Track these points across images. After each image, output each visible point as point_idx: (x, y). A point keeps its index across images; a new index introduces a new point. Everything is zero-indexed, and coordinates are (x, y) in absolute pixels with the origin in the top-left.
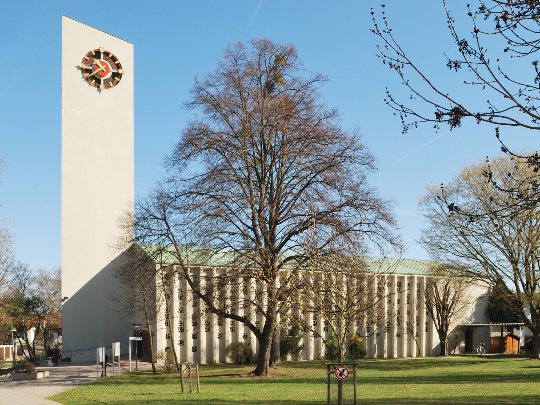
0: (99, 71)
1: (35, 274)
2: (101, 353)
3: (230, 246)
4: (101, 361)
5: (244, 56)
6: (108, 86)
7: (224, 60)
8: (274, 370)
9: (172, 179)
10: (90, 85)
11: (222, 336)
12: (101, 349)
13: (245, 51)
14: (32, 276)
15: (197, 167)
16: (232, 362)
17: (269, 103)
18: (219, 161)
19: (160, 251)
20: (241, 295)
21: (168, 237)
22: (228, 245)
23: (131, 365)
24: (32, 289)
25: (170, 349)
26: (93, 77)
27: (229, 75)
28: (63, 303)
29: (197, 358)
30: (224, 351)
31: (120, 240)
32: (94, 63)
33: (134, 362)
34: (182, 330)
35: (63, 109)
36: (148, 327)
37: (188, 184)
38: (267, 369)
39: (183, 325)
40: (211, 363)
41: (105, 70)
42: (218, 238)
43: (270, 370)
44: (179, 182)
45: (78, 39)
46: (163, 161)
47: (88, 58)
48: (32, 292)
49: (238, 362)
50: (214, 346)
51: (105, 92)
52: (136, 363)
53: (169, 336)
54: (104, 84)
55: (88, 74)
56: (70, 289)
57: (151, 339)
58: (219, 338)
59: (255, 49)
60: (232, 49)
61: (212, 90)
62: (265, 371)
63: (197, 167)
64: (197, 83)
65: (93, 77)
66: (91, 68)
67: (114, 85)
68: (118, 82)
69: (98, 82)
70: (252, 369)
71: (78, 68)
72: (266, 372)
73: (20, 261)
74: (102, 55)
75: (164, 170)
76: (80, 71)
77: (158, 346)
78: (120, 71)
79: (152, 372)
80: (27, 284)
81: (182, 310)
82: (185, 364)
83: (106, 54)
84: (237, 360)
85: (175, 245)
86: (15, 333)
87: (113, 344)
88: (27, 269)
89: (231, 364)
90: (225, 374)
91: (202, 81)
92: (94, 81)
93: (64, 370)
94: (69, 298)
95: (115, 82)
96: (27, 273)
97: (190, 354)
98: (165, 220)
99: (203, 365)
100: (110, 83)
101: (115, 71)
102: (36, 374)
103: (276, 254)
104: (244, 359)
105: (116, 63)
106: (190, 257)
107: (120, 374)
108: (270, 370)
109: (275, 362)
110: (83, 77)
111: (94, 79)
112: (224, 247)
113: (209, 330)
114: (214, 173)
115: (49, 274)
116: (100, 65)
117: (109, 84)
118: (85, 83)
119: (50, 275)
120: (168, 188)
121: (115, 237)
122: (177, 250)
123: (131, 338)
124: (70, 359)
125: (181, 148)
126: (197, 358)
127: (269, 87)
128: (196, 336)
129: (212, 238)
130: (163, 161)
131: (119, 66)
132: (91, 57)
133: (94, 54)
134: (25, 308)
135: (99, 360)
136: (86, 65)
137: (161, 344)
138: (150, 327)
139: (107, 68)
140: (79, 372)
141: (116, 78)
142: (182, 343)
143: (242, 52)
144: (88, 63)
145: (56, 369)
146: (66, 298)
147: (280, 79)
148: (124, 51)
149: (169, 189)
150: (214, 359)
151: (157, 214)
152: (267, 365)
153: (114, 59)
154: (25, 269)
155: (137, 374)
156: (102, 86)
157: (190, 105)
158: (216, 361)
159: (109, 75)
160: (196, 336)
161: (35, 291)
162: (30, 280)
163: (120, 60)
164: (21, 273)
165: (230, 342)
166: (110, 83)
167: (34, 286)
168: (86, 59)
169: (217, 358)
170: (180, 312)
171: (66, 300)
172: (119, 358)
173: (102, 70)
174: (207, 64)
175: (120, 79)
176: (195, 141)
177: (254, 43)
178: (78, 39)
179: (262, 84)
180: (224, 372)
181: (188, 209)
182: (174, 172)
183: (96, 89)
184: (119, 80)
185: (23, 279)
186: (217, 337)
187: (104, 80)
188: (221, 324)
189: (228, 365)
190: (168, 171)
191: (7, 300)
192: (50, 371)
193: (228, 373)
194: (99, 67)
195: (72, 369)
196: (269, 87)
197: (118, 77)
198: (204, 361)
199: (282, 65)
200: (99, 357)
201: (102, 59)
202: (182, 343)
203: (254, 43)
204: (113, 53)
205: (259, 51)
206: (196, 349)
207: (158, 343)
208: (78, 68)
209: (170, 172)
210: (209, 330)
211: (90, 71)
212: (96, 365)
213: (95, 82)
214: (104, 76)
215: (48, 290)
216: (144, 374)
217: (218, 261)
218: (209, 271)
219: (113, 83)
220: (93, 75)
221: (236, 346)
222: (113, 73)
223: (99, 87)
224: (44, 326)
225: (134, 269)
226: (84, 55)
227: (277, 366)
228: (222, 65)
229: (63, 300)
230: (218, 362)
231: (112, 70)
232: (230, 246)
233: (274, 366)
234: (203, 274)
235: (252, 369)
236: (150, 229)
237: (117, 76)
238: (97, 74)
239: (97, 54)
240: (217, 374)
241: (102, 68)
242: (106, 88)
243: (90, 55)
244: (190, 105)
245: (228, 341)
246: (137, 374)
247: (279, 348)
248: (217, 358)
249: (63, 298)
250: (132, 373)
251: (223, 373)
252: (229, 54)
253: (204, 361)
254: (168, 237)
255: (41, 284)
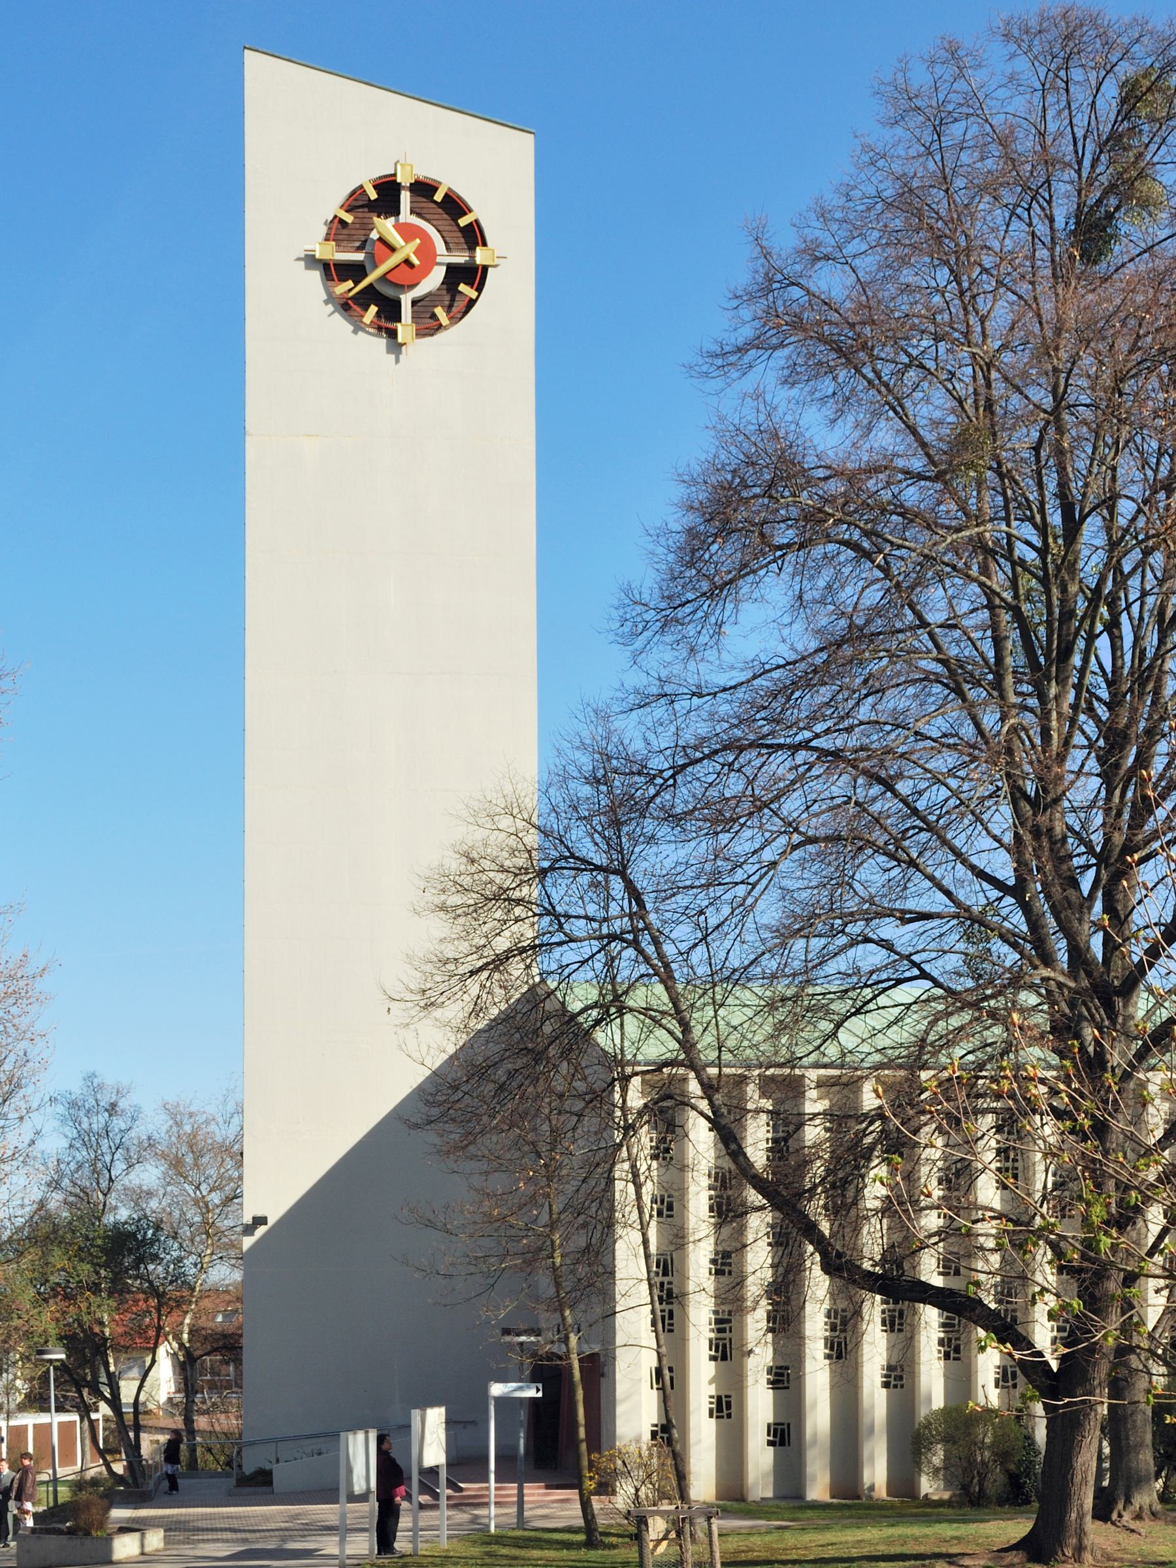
0: (395, 266)
1: (153, 1123)
2: (360, 1455)
3: (924, 975)
4: (359, 1487)
5: (973, 105)
6: (428, 327)
7: (881, 137)
8: (1123, 1537)
9: (655, 690)
10: (358, 328)
11: (900, 1375)
12: (361, 1436)
13: (977, 77)
14: (140, 1131)
15: (766, 624)
16: (946, 1496)
17: (1081, 302)
18: (863, 591)
19: (613, 1005)
20: (988, 1192)
21: (635, 944)
22: (916, 972)
23: (498, 1502)
24: (142, 1188)
25: (669, 1434)
26: (369, 296)
27: (908, 199)
28: (248, 1242)
29: (790, 1473)
30: (910, 1442)
31: (429, 968)
32: (374, 235)
33: (512, 1489)
34: (726, 1349)
35: (248, 439)
36: (566, 1340)
37: (724, 709)
38: (1081, 1533)
39: (727, 1325)
40: (850, 1498)
41: (416, 261)
42: (867, 940)
43: (1098, 1535)
44: (686, 704)
45: (311, 137)
46: (615, 614)
47: (349, 218)
48: (139, 1196)
49: (971, 1499)
50: (865, 1421)
51: (420, 351)
52: (521, 1495)
53: (669, 1380)
54: (416, 317)
55: (350, 284)
56: (273, 1189)
57: (580, 1394)
58: (886, 1385)
59: (1022, 64)
60: (920, 78)
61: (832, 282)
62: (1073, 1541)
63: (766, 624)
64: (767, 255)
65: (369, 296)
66: (359, 257)
67: (455, 319)
68: (472, 303)
69: (390, 310)
70: (1017, 1528)
71: (311, 261)
72: (1080, 1549)
73: (94, 1075)
74: (405, 198)
75: (621, 656)
76: (316, 275)
77: (619, 1423)
78: (481, 256)
79: (581, 1537)
80: (119, 1167)
81: (727, 1264)
82: (662, 1514)
83: (423, 189)
84: (965, 1488)
85: (667, 979)
86: (62, 1367)
87: (416, 1414)
88: (123, 1104)
89: (940, 1503)
90: (897, 1549)
91: (785, 242)
92: (373, 309)
93: (235, 1524)
94: (271, 1221)
95: (460, 304)
96: (119, 1123)
97: (760, 1457)
98: (622, 872)
99: (816, 1506)
100: (440, 312)
101: (460, 259)
102: (108, 1540)
103: (1119, 1002)
104: (996, 1480)
105: (463, 222)
106: (737, 1024)
107: (445, 1544)
108: (1098, 1535)
109: (1128, 1501)
110: (331, 298)
111: (369, 296)
112: (899, 982)
113: (843, 1349)
114: (846, 649)
115: (207, 1122)
116: (396, 239)
117: (434, 316)
118: (340, 324)
119: (213, 1127)
120: (636, 734)
121: (409, 958)
122: (675, 1002)
123: (497, 1389)
124: (269, 1473)
125: (693, 549)
126: (790, 1473)
127: (1092, 233)
128: (785, 1379)
129: (842, 940)
130: (615, 614)
131: (473, 236)
132: (363, 213)
133: (373, 195)
134: (101, 1269)
135: (350, 1483)
136: (340, 247)
137: (635, 1413)
138: (573, 1339)
139: (426, 252)
140: (286, 1533)
141: (462, 287)
142: (726, 1407)
143: (961, 85)
144: (350, 238)
145: (206, 1517)
146: (260, 1221)
147: (1143, 187)
148: (492, 168)
149: (644, 736)
150: (867, 1478)
151: (588, 849)
152: (1081, 1517)
153: (454, 206)
154: (113, 1105)
155: (519, 1543)
156: (405, 329)
157: (729, 358)
158: (872, 1488)
159: (434, 280)
160: (785, 1379)
161: (150, 1194)
162: (133, 1149)
163: (481, 211)
164: (98, 1124)
165: (938, 1401)
166: (440, 312)
167: (149, 1175)
168: (343, 223)
169: (876, 1473)
170: (718, 1273)
171: (261, 1231)
172: (443, 1474)
173: (407, 262)
174: (807, 169)
175: (479, 290)
176: (746, 515)
177: (1016, 35)
178: (311, 137)
179: (1060, 222)
180: (889, 1541)
181: (721, 817)
182: (662, 657)
183: (382, 342)
184: (473, 294)
185: (105, 1143)
186: (879, 1380)
187: (414, 303)
188: (895, 1323)
189: (928, 1510)
190: (636, 655)
191: (42, 1234)
192: (171, 1527)
193: (906, 1550)
194: (393, 249)
195: (266, 1518)
196: (1092, 233)
197: (470, 284)
198: (818, 1489)
199: (1152, 119)
200: (350, 1471)
201: (406, 216)
202: (726, 1407)
203: (1016, 35)
204: (449, 180)
205: (1042, 71)
206: (784, 1435)
207: (620, 1410)
208: (311, 261)
209: (645, 660)
210: (843, 1349)
211: (355, 271)
212: (337, 1502)
213: (378, 315)
214: (412, 286)
215: (204, 1188)
216: (551, 1544)
217: (881, 1041)
218: (843, 1086)
219: (449, 309)
220: (371, 286)
221: (960, 1421)
222: (451, 269)
223: (392, 334)
224: (185, 1336)
225: (521, 1092)
226: (332, 205)
227: (1138, 1517)
228: (876, 158)
229: (249, 1230)
230: (881, 1492)
231: (445, 256)
232: (924, 975)
233: (1127, 1516)
234: (814, 1103)
235: (1017, 1528)
236: (557, 916)
237: (467, 277)
238: (384, 278)
239: (387, 195)
240: (855, 1553)
241: (407, 250)
242: (422, 333)
243: (357, 202)
244: (729, 358)
245: (929, 1400)
246: (519, 1543)
247: (1149, 1437)
248: (876, 1473)
249: (247, 1219)
250: (499, 1540)
251: (883, 1549)
252: (905, 104)
253: (818, 1489)
254: (635, 944)
255: (176, 1164)
